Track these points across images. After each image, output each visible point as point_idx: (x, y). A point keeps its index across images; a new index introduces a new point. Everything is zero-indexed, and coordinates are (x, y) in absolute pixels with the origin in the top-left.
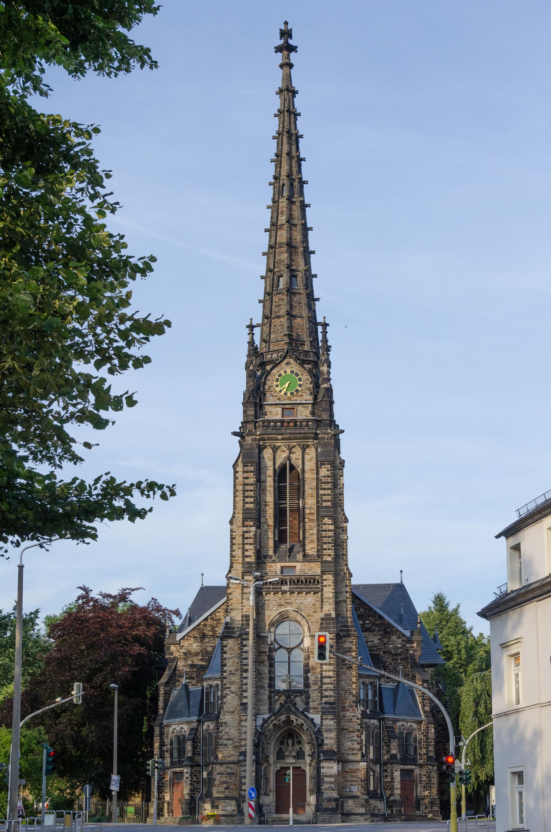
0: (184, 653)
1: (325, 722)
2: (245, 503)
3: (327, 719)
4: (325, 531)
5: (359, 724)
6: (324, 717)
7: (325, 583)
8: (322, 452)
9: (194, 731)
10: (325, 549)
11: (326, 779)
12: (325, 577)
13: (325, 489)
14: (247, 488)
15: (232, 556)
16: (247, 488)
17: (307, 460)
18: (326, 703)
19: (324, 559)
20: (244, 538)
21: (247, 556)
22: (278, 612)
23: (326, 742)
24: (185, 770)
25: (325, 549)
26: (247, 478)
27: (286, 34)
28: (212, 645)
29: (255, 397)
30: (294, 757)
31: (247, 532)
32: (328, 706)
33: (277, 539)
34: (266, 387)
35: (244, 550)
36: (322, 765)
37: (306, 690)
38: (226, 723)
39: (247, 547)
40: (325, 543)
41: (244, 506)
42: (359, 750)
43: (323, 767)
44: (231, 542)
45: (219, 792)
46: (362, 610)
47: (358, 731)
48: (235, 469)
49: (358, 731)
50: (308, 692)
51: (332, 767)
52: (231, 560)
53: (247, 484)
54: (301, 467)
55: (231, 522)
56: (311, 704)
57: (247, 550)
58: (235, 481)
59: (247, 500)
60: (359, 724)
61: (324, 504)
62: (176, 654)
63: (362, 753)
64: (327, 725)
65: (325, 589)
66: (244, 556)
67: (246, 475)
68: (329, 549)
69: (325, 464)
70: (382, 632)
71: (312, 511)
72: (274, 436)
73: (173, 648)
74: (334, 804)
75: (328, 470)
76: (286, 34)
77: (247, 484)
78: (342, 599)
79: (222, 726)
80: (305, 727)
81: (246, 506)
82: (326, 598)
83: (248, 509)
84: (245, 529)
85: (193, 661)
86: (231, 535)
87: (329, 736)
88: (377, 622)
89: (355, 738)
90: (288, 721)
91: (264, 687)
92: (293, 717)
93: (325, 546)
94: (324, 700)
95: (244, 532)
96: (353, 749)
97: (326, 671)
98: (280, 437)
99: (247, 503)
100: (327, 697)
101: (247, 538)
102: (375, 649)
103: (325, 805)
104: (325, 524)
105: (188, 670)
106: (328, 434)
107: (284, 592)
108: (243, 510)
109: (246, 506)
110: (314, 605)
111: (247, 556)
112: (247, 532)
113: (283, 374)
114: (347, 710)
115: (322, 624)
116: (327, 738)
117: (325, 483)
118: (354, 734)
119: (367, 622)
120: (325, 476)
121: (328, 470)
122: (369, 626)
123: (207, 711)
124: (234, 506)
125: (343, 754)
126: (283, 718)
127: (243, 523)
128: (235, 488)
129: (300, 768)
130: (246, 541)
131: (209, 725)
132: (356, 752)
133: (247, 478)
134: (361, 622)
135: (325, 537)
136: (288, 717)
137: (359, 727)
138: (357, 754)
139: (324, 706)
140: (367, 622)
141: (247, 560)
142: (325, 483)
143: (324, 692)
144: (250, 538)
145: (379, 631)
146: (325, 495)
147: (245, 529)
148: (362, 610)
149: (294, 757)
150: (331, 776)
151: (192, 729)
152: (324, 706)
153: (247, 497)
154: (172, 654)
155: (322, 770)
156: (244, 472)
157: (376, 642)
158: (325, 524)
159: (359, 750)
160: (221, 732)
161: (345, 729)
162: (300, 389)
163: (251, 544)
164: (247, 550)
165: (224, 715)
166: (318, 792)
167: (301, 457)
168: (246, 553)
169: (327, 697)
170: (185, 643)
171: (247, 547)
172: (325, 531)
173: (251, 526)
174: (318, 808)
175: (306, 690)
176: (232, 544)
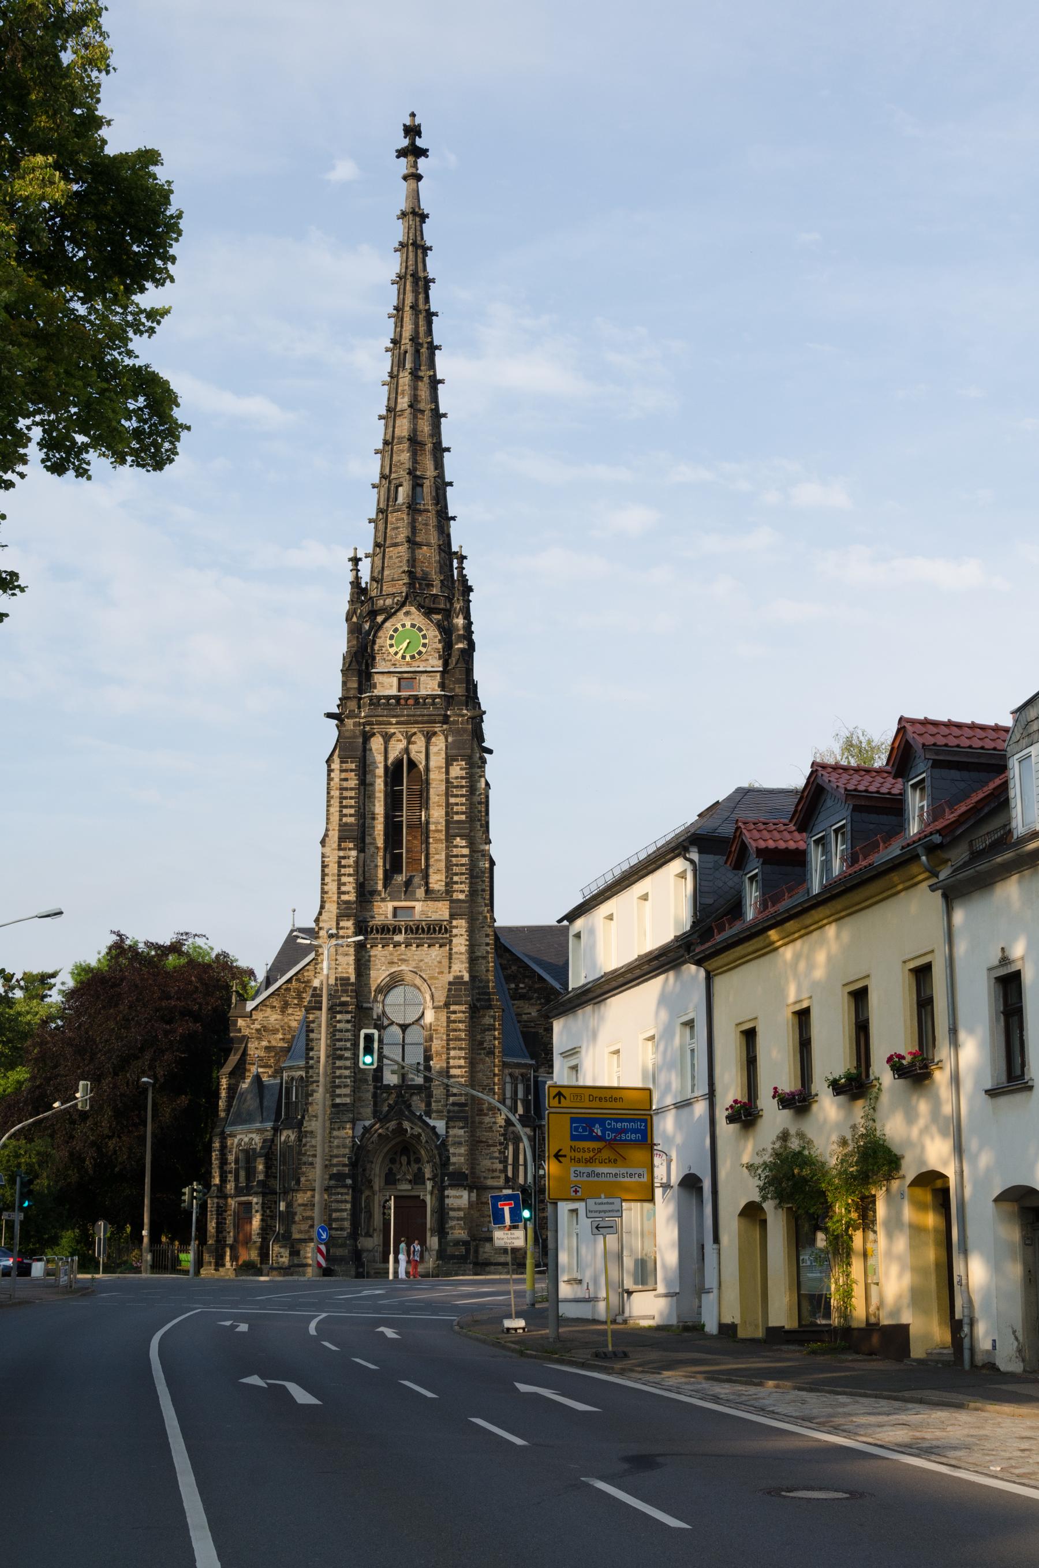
0: (257, 1030)
1: (451, 1132)
2: (342, 816)
3: (454, 1127)
4: (456, 856)
5: (503, 1135)
6: (451, 1124)
7: (455, 931)
8: (454, 741)
9: (269, 1146)
10: (456, 883)
11: (452, 1214)
12: (455, 923)
13: (457, 796)
14: (346, 794)
15: (323, 892)
16: (346, 794)
17: (434, 754)
18: (454, 1104)
19: (454, 897)
20: (340, 866)
21: (344, 893)
22: (388, 973)
23: (453, 1160)
24: (255, 1200)
25: (456, 883)
26: (346, 780)
27: (413, 131)
28: (297, 1018)
29: (360, 662)
30: (410, 1181)
31: (344, 858)
32: (456, 1108)
33: (388, 867)
34: (376, 647)
35: (340, 884)
36: (446, 1193)
37: (427, 1085)
38: (312, 1132)
39: (344, 879)
40: (456, 874)
41: (341, 820)
42: (501, 1171)
43: (448, 1197)
44: (323, 871)
45: (300, 1232)
46: (514, 968)
47: (501, 1144)
48: (329, 766)
49: (501, 1144)
50: (430, 1087)
51: (461, 1197)
52: (322, 897)
53: (346, 789)
54: (424, 763)
55: (323, 843)
56: (434, 1106)
57: (344, 884)
58: (328, 784)
59: (345, 811)
60: (503, 1135)
61: (456, 818)
62: (246, 1032)
63: (506, 1176)
64: (455, 1136)
65: (455, 940)
66: (340, 893)
67: (344, 775)
68: (461, 883)
69: (457, 760)
70: (543, 1001)
71: (440, 828)
72: (385, 719)
73: (241, 1022)
74: (463, 1249)
75: (461, 769)
76: (413, 131)
77: (346, 789)
78: (479, 954)
79: (306, 1137)
80: (423, 1139)
81: (344, 819)
82: (456, 953)
83: (346, 824)
84: (341, 853)
85: (269, 1042)
86: (323, 862)
87: (457, 1151)
88: (537, 986)
89: (497, 1155)
90: (400, 1130)
91: (366, 1081)
92: (406, 1125)
93: (456, 878)
94: (451, 1099)
95: (341, 858)
96: (494, 1171)
97: (454, 1058)
98: (394, 720)
99: (346, 815)
100: (455, 1095)
101: (344, 867)
102: (532, 1024)
103: (450, 1250)
104: (456, 847)
105: (262, 1054)
106: (463, 716)
107: (397, 945)
108: (340, 825)
109: (344, 819)
110: (440, 962)
111: (344, 893)
112: (344, 858)
113: (400, 629)
114: (486, 1115)
115: (449, 990)
116: (454, 1154)
117: (457, 787)
118: (495, 1149)
119: (521, 985)
120: (457, 778)
121: (461, 769)
122: (524, 991)
123: (287, 1114)
124: (328, 819)
125: (479, 1178)
126: (392, 1125)
127: (339, 845)
128: (328, 793)
129: (419, 1197)
130: (343, 871)
131: (287, 1136)
132: (497, 1174)
133: (346, 780)
134: (513, 986)
135: (457, 865)
136: (400, 1124)
137: (502, 1138)
138: (499, 1177)
139: (452, 1108)
140: (521, 985)
141: (345, 897)
142: (457, 787)
143: (451, 1089)
144: (349, 866)
145: (539, 998)
146: (457, 804)
147: (341, 853)
148: (514, 968)
149: (410, 1181)
150: (459, 1209)
151: (265, 1141)
152: (452, 1108)
153: (346, 807)
154: (240, 1031)
155: (447, 1201)
156: (342, 771)
157: (534, 1014)
158: (456, 847)
159: (501, 1171)
160: (305, 1145)
161: (482, 1142)
162: (424, 650)
163: (350, 875)
164: (344, 884)
165: (310, 1120)
166: (441, 1231)
167: (423, 750)
168: (343, 889)
169: (455, 1095)
170: (258, 1016)
171: (344, 879)
172: (456, 856)
173: (350, 849)
174: (441, 1254)
175: (427, 1085)
176: (324, 875)
